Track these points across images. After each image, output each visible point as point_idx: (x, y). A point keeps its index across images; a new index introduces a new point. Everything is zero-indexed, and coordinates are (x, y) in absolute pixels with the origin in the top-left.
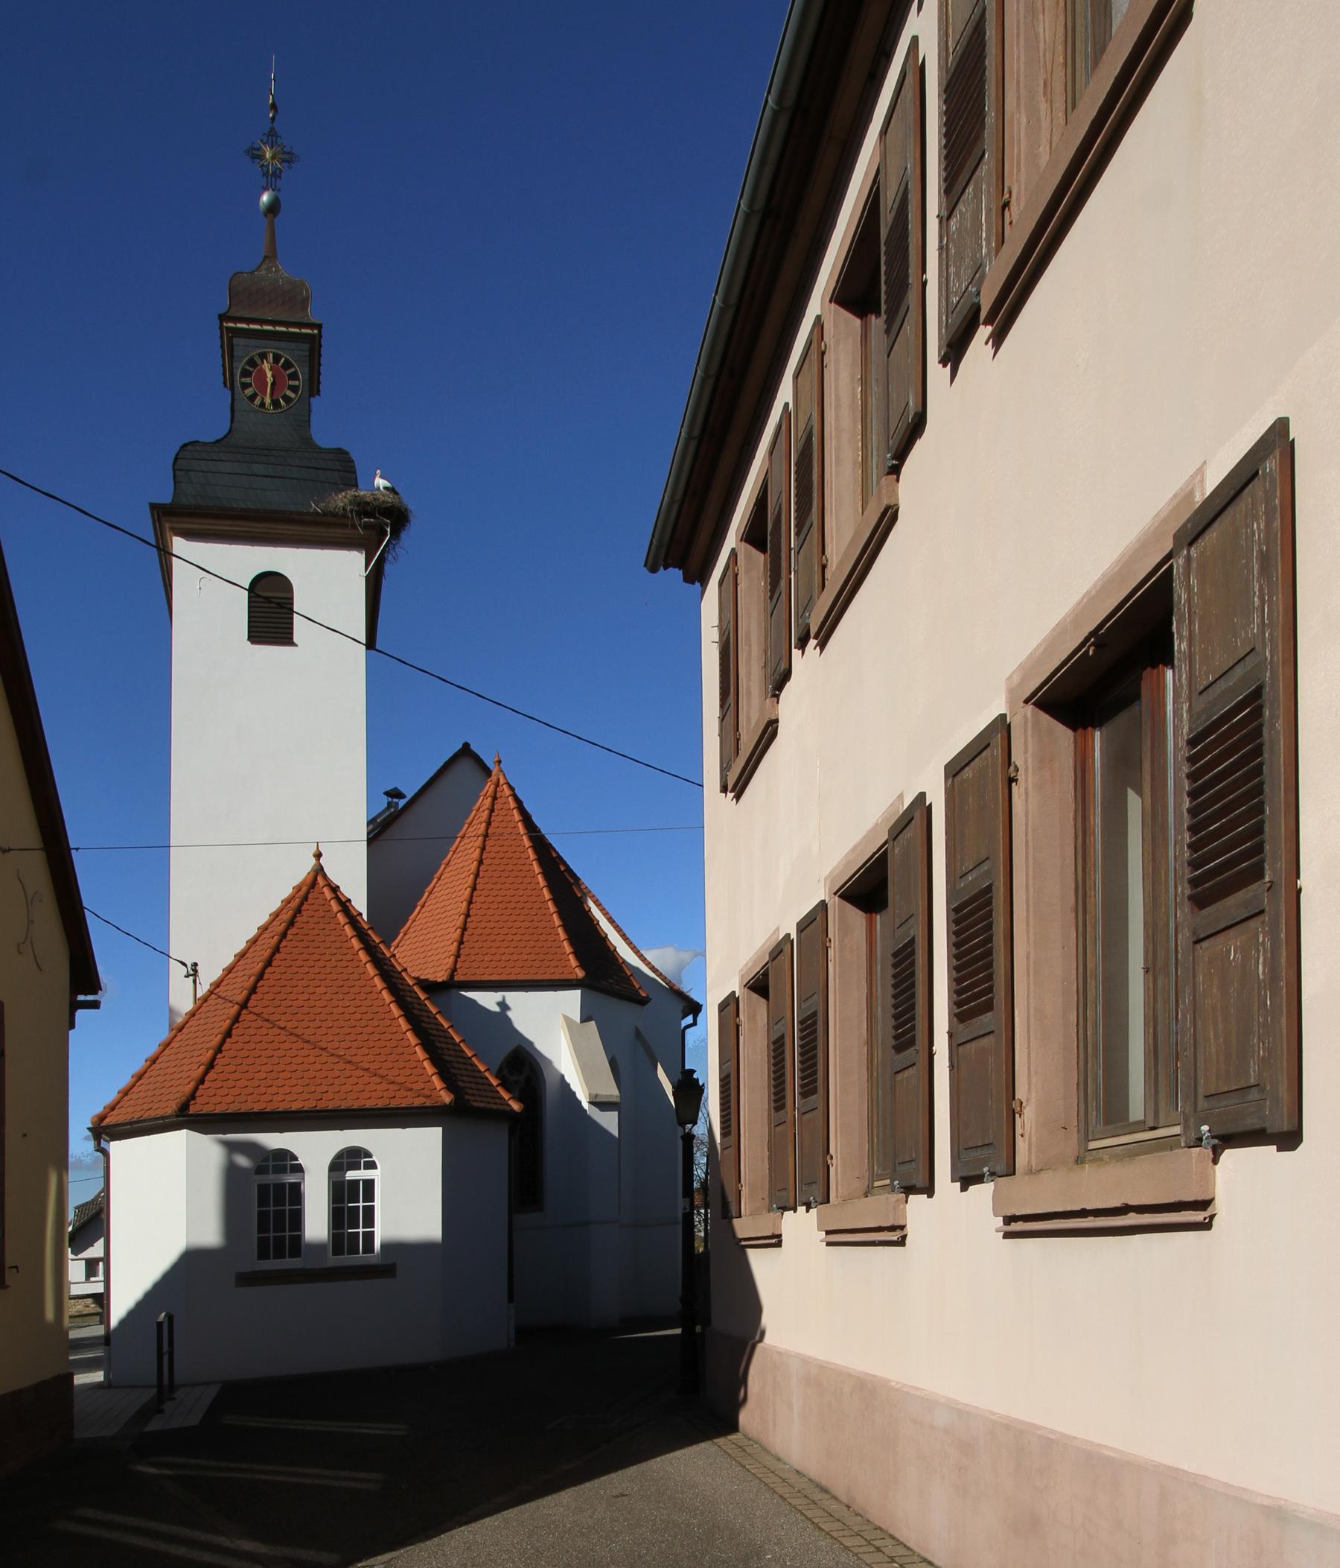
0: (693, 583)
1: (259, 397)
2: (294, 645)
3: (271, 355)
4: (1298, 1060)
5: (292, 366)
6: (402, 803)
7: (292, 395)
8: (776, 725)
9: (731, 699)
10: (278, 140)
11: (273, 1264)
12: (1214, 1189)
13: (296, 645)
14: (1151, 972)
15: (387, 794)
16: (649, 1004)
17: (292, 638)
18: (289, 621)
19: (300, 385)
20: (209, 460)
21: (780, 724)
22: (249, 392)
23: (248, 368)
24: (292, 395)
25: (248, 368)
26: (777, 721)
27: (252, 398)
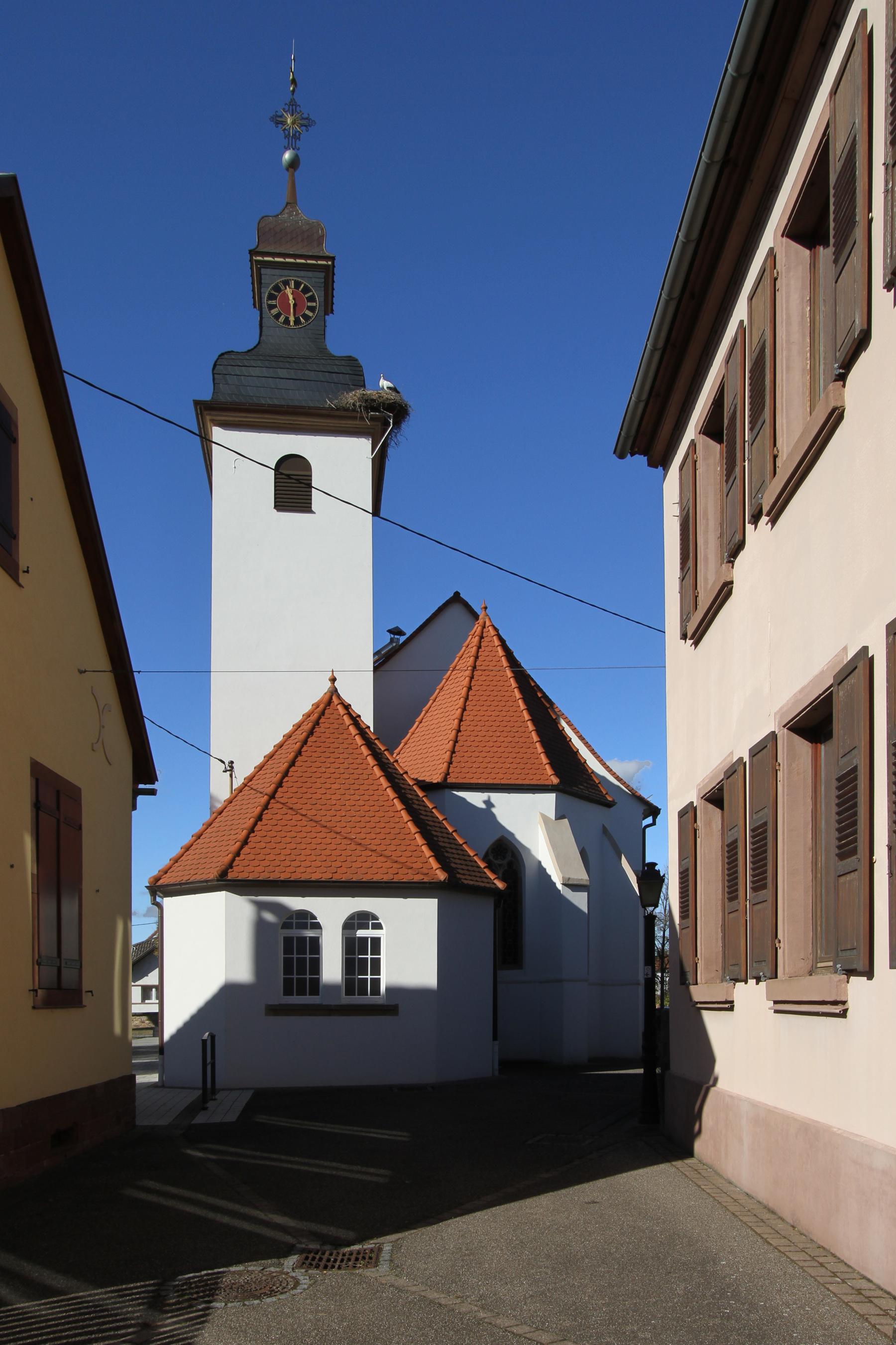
0: (657, 468)
1: (282, 316)
2: (312, 512)
3: (293, 282)
6: (402, 639)
7: (310, 314)
8: (730, 586)
9: (691, 563)
10: (298, 108)
11: (296, 999)
13: (314, 513)
15: (390, 631)
16: (614, 807)
17: (311, 507)
21: (734, 585)
22: (274, 311)
23: (273, 292)
24: (310, 314)
25: (273, 292)
26: (732, 583)
27: (277, 316)
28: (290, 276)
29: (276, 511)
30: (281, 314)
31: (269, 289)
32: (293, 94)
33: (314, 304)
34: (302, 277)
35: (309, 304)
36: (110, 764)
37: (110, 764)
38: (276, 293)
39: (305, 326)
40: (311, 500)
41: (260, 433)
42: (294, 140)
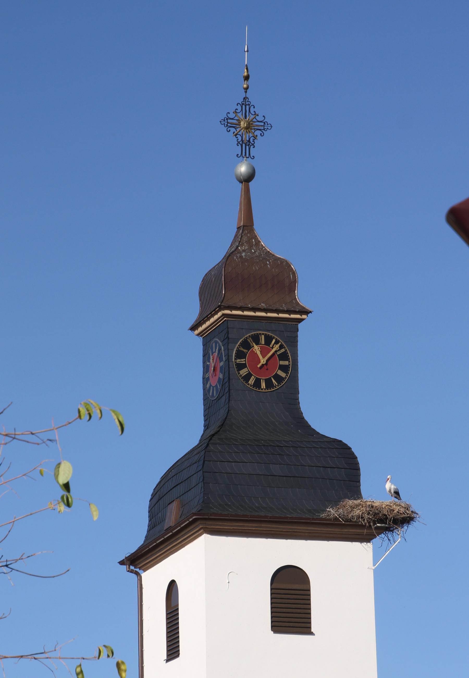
2: (312, 634)
3: (263, 336)
4: (176, 610)
5: (272, 338)
7: (282, 374)
12: (331, 438)
14: (36, 656)
17: (310, 628)
18: (306, 616)
19: (290, 365)
20: (240, 462)
22: (244, 372)
23: (242, 349)
24: (282, 374)
25: (242, 349)
27: (247, 377)
28: (261, 330)
29: (272, 632)
30: (246, 367)
31: (237, 346)
32: (246, 92)
33: (286, 363)
34: (273, 331)
35: (282, 363)
36: (4, 458)
37: (4, 458)
38: (245, 351)
39: (278, 389)
40: (310, 623)
41: (248, 538)
42: (247, 147)
